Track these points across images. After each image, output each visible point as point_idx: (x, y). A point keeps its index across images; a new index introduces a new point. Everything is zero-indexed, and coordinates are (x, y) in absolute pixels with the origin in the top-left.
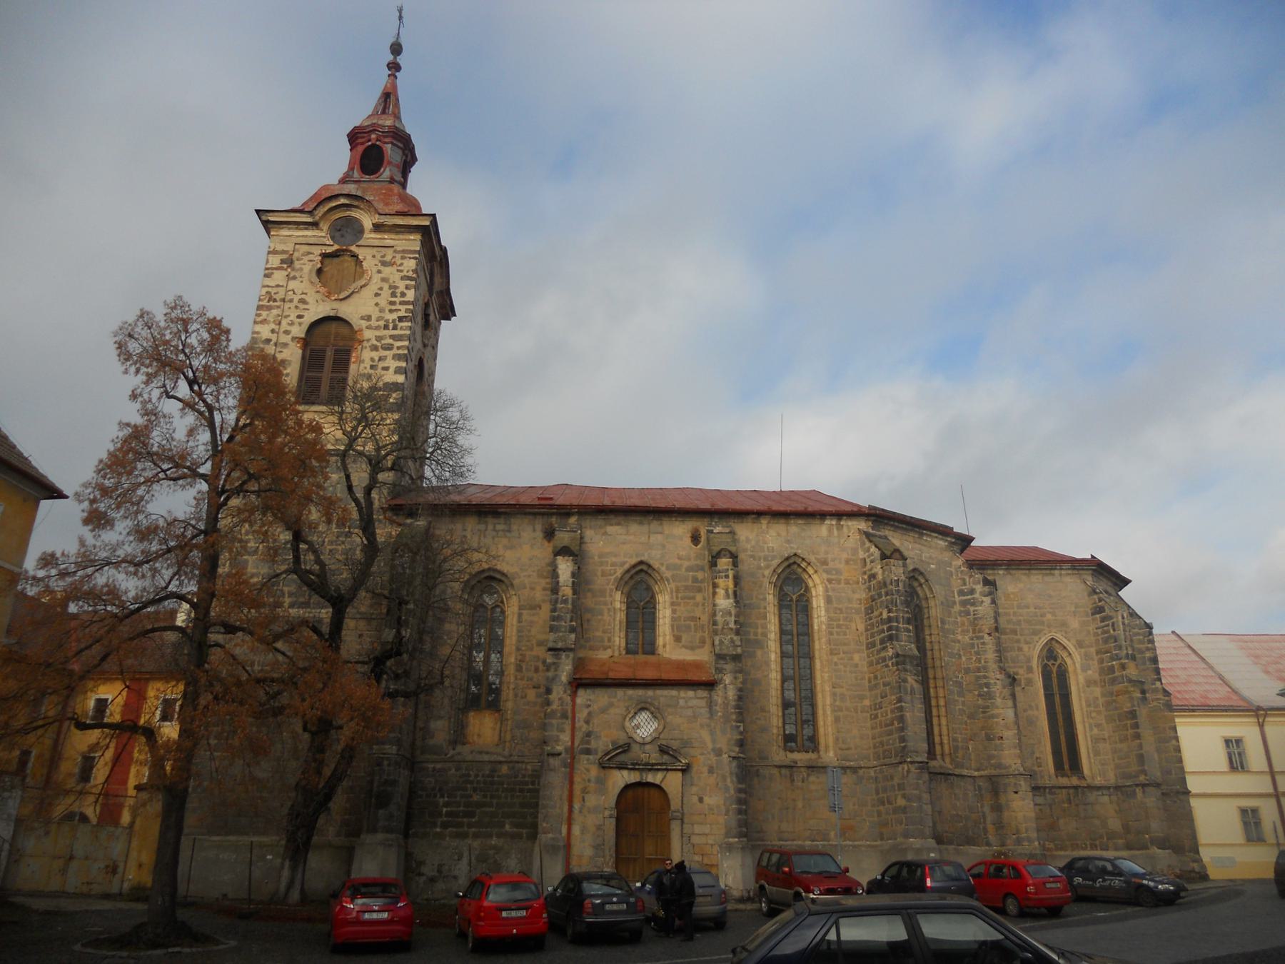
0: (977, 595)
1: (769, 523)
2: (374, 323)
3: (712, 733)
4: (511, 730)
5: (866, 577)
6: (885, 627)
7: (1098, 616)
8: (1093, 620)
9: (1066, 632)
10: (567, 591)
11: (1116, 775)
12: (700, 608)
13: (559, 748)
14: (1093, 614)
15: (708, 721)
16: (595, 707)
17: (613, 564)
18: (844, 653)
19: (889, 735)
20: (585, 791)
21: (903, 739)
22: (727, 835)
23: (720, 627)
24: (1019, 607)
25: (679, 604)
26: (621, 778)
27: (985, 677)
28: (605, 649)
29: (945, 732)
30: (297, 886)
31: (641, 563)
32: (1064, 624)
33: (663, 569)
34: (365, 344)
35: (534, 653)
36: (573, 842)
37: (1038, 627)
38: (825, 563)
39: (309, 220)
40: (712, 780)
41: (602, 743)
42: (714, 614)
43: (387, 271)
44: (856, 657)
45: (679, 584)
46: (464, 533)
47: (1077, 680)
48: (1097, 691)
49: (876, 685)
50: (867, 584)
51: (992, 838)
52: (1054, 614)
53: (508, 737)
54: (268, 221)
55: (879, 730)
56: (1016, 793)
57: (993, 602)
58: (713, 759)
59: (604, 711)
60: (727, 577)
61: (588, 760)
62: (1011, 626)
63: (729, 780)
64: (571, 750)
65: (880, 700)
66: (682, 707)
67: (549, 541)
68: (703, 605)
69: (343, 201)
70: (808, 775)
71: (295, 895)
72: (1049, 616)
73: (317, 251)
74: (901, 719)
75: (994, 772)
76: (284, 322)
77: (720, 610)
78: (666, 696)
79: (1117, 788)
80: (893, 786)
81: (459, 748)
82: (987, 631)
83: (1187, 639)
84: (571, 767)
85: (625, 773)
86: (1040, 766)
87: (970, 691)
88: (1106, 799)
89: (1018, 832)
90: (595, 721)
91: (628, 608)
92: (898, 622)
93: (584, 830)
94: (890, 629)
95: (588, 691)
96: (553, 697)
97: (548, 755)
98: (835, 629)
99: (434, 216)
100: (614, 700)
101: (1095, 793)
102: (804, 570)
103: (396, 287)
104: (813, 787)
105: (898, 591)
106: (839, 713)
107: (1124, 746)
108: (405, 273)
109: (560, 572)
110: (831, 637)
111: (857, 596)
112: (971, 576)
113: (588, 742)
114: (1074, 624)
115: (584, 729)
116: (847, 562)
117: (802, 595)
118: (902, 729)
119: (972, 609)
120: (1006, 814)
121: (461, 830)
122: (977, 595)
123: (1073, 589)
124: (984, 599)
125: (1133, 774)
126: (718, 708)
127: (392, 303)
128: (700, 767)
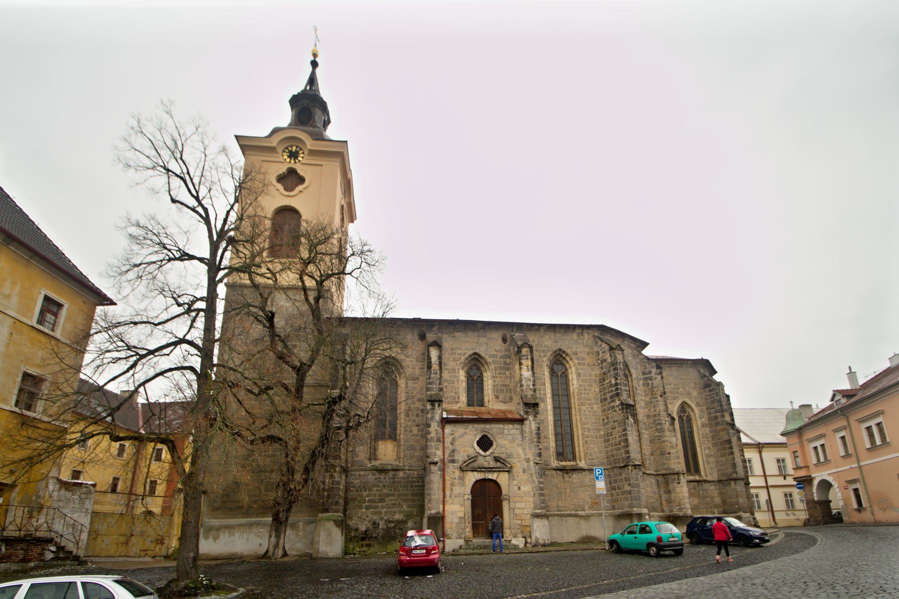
0: (653, 375)
1: (545, 331)
3: (524, 449)
4: (404, 451)
5: (599, 362)
6: (614, 389)
7: (707, 389)
8: (704, 391)
11: (718, 474)
12: (509, 379)
13: (436, 460)
14: (704, 388)
15: (521, 442)
16: (456, 435)
17: (459, 354)
18: (589, 405)
19: (617, 450)
22: (535, 508)
23: (525, 388)
25: (497, 377)
26: (472, 477)
27: (659, 420)
30: (281, 547)
31: (475, 353)
32: (689, 394)
33: (487, 357)
35: (415, 406)
37: (676, 395)
38: (576, 354)
40: (525, 477)
41: (461, 457)
42: (521, 381)
44: (595, 407)
45: (496, 366)
47: (697, 424)
48: (707, 430)
49: (607, 423)
50: (600, 365)
52: (684, 388)
53: (402, 456)
54: (246, 145)
55: (611, 448)
56: (678, 483)
57: (662, 378)
60: (527, 359)
61: (453, 466)
63: (534, 477)
64: (443, 461)
65: (611, 431)
67: (422, 341)
68: (510, 377)
71: (280, 552)
72: (681, 389)
74: (626, 440)
77: (524, 378)
78: (496, 428)
80: (622, 479)
82: (659, 394)
84: (443, 470)
85: (475, 473)
87: (651, 428)
88: (713, 487)
90: (457, 443)
91: (468, 380)
92: (621, 385)
94: (617, 389)
95: (452, 425)
97: (430, 463)
98: (583, 392)
100: (468, 431)
102: (564, 358)
104: (575, 481)
106: (588, 439)
107: (723, 459)
109: (432, 356)
111: (594, 373)
112: (649, 364)
113: (453, 456)
114: (695, 394)
115: (450, 448)
116: (588, 353)
118: (627, 446)
119: (650, 382)
120: (673, 495)
121: (378, 510)
122: (653, 375)
123: (693, 375)
124: (657, 376)
125: (729, 474)
126: (526, 435)
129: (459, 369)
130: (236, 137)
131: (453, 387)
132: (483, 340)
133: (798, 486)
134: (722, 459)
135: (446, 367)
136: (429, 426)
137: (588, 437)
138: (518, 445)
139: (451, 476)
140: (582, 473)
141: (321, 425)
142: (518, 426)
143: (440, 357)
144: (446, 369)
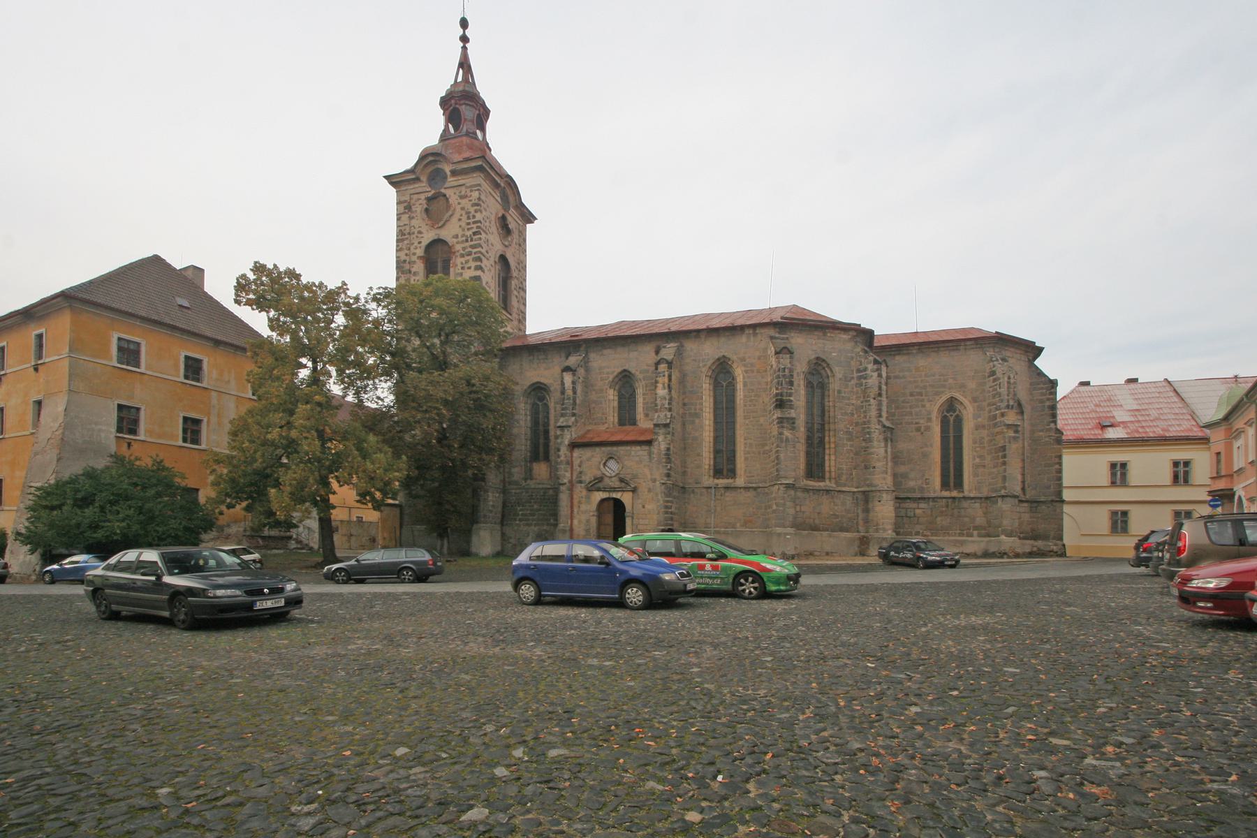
0: (868, 372)
2: (460, 239)
9: (964, 392)
10: (569, 392)
13: (565, 481)
16: (584, 458)
17: (608, 373)
21: (777, 470)
24: (926, 376)
26: (599, 496)
27: (868, 428)
28: (603, 424)
29: (833, 463)
31: (625, 370)
32: (963, 386)
33: (637, 373)
34: (457, 254)
36: (574, 527)
39: (413, 177)
41: (587, 478)
43: (464, 202)
46: (929, 424)
51: (861, 528)
52: (955, 379)
54: (393, 180)
58: (651, 484)
59: (588, 460)
62: (917, 390)
64: (571, 482)
69: (431, 158)
72: (951, 381)
73: (423, 196)
75: (867, 489)
76: (412, 248)
79: (987, 498)
81: (528, 481)
83: (1176, 386)
85: (601, 493)
86: (927, 484)
89: (877, 524)
91: (620, 398)
93: (580, 522)
96: (561, 453)
101: (969, 501)
103: (470, 213)
105: (784, 376)
108: (473, 202)
113: (581, 477)
117: (730, 383)
119: (864, 381)
120: (871, 514)
122: (868, 372)
124: (873, 374)
127: (468, 224)
128: (643, 489)
130: (385, 177)
132: (633, 355)
133: (1212, 503)
134: (994, 470)
136: (559, 450)
138: (645, 466)
142: (647, 448)
143: (574, 383)
144: (594, 390)
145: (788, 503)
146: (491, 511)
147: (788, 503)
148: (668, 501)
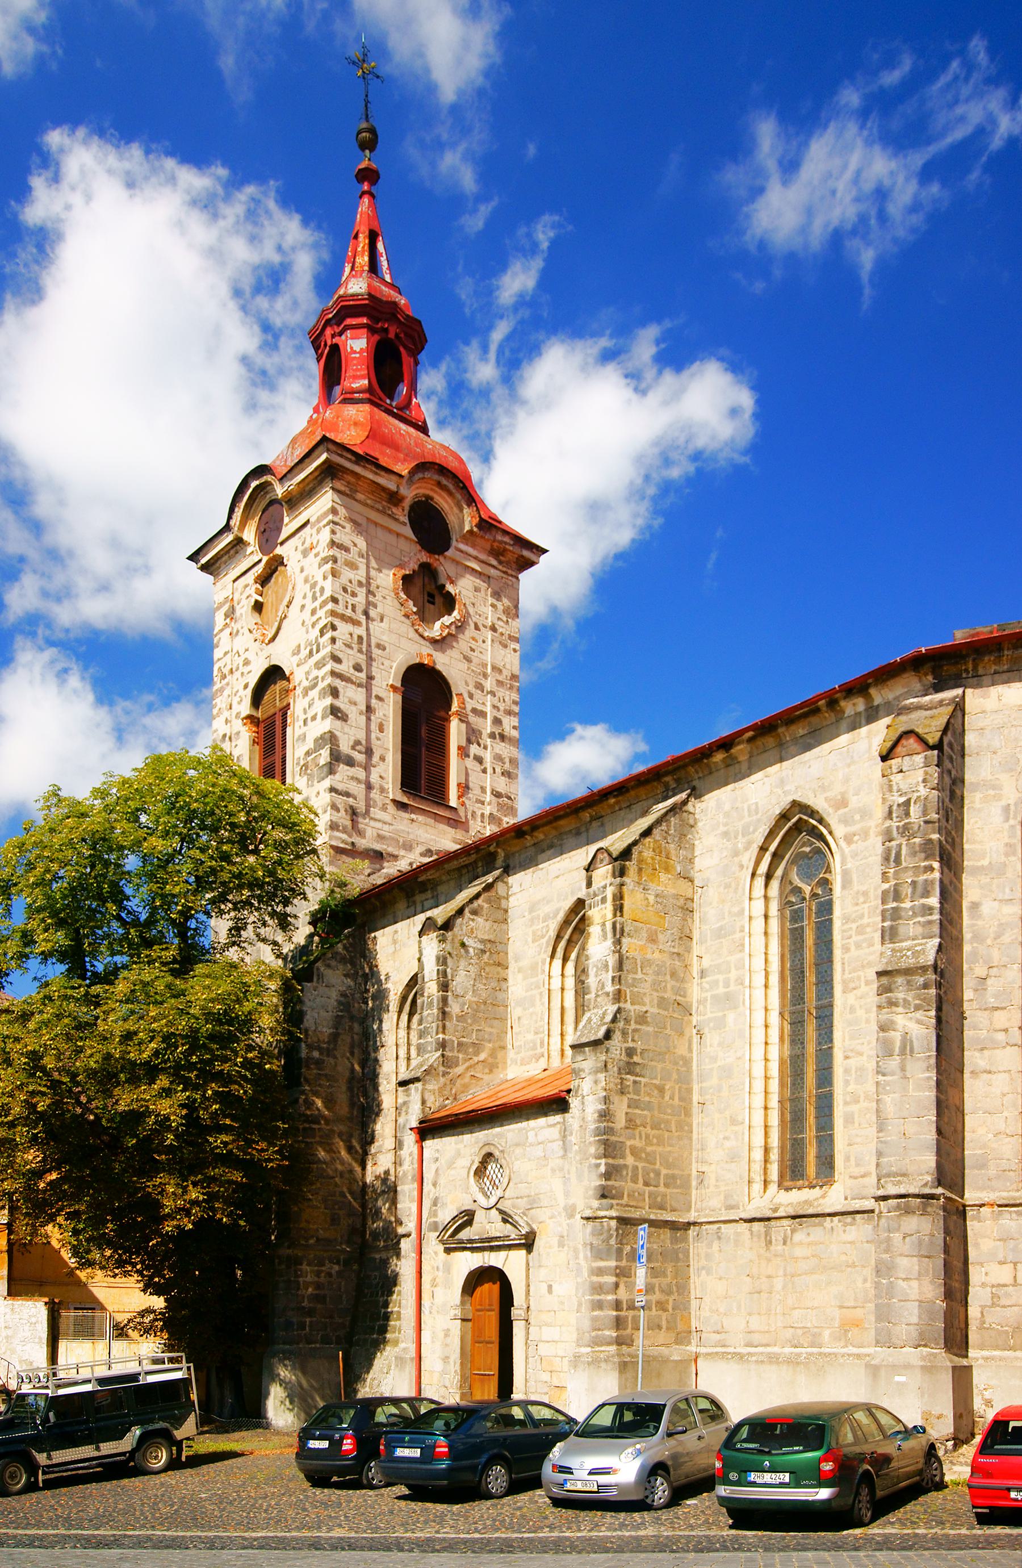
3: (566, 1180)
15: (560, 1162)
20: (434, 1284)
26: (468, 1262)
63: (581, 1256)
66: (531, 1145)
70: (793, 1231)
99: (325, 439)
105: (906, 828)
108: (322, 555)
110: (846, 956)
129: (544, 963)
130: (547, 551)
131: (531, 1014)
135: (521, 964)
137: (857, 1101)
138: (553, 1170)
139: (433, 1262)
140: (821, 1225)
141: (477, 1150)
143: (442, 960)
145: (904, 1262)
146: (310, 1313)
147: (904, 1262)
148: (600, 1272)
